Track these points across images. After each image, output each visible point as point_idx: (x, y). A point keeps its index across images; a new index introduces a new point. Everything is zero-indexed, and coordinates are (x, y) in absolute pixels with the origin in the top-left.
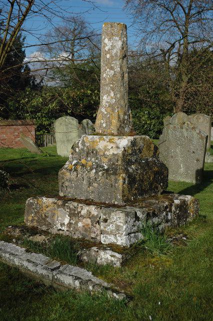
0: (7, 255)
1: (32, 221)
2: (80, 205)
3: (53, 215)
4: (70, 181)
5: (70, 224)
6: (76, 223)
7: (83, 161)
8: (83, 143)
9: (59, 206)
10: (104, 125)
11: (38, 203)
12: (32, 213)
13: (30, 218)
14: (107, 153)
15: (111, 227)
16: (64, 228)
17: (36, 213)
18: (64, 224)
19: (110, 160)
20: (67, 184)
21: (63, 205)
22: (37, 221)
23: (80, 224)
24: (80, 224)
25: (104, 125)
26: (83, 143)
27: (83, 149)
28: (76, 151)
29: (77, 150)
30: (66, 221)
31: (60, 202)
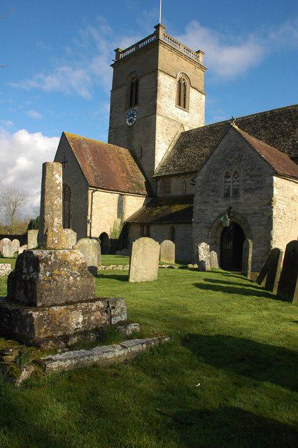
0: (86, 358)
1: (45, 332)
2: (89, 304)
3: (68, 319)
4: (50, 290)
5: (84, 321)
6: (89, 318)
7: (56, 272)
8: (56, 257)
9: (71, 310)
10: (56, 242)
11: (49, 314)
12: (44, 324)
13: (43, 330)
14: (77, 263)
15: (118, 311)
16: (80, 326)
17: (49, 324)
18: (79, 323)
19: (80, 268)
20: (46, 293)
21: (76, 309)
22: (51, 331)
23: (92, 318)
24: (92, 318)
25: (56, 242)
26: (56, 257)
27: (55, 262)
28: (48, 264)
29: (50, 263)
30: (81, 319)
31: (72, 307)
